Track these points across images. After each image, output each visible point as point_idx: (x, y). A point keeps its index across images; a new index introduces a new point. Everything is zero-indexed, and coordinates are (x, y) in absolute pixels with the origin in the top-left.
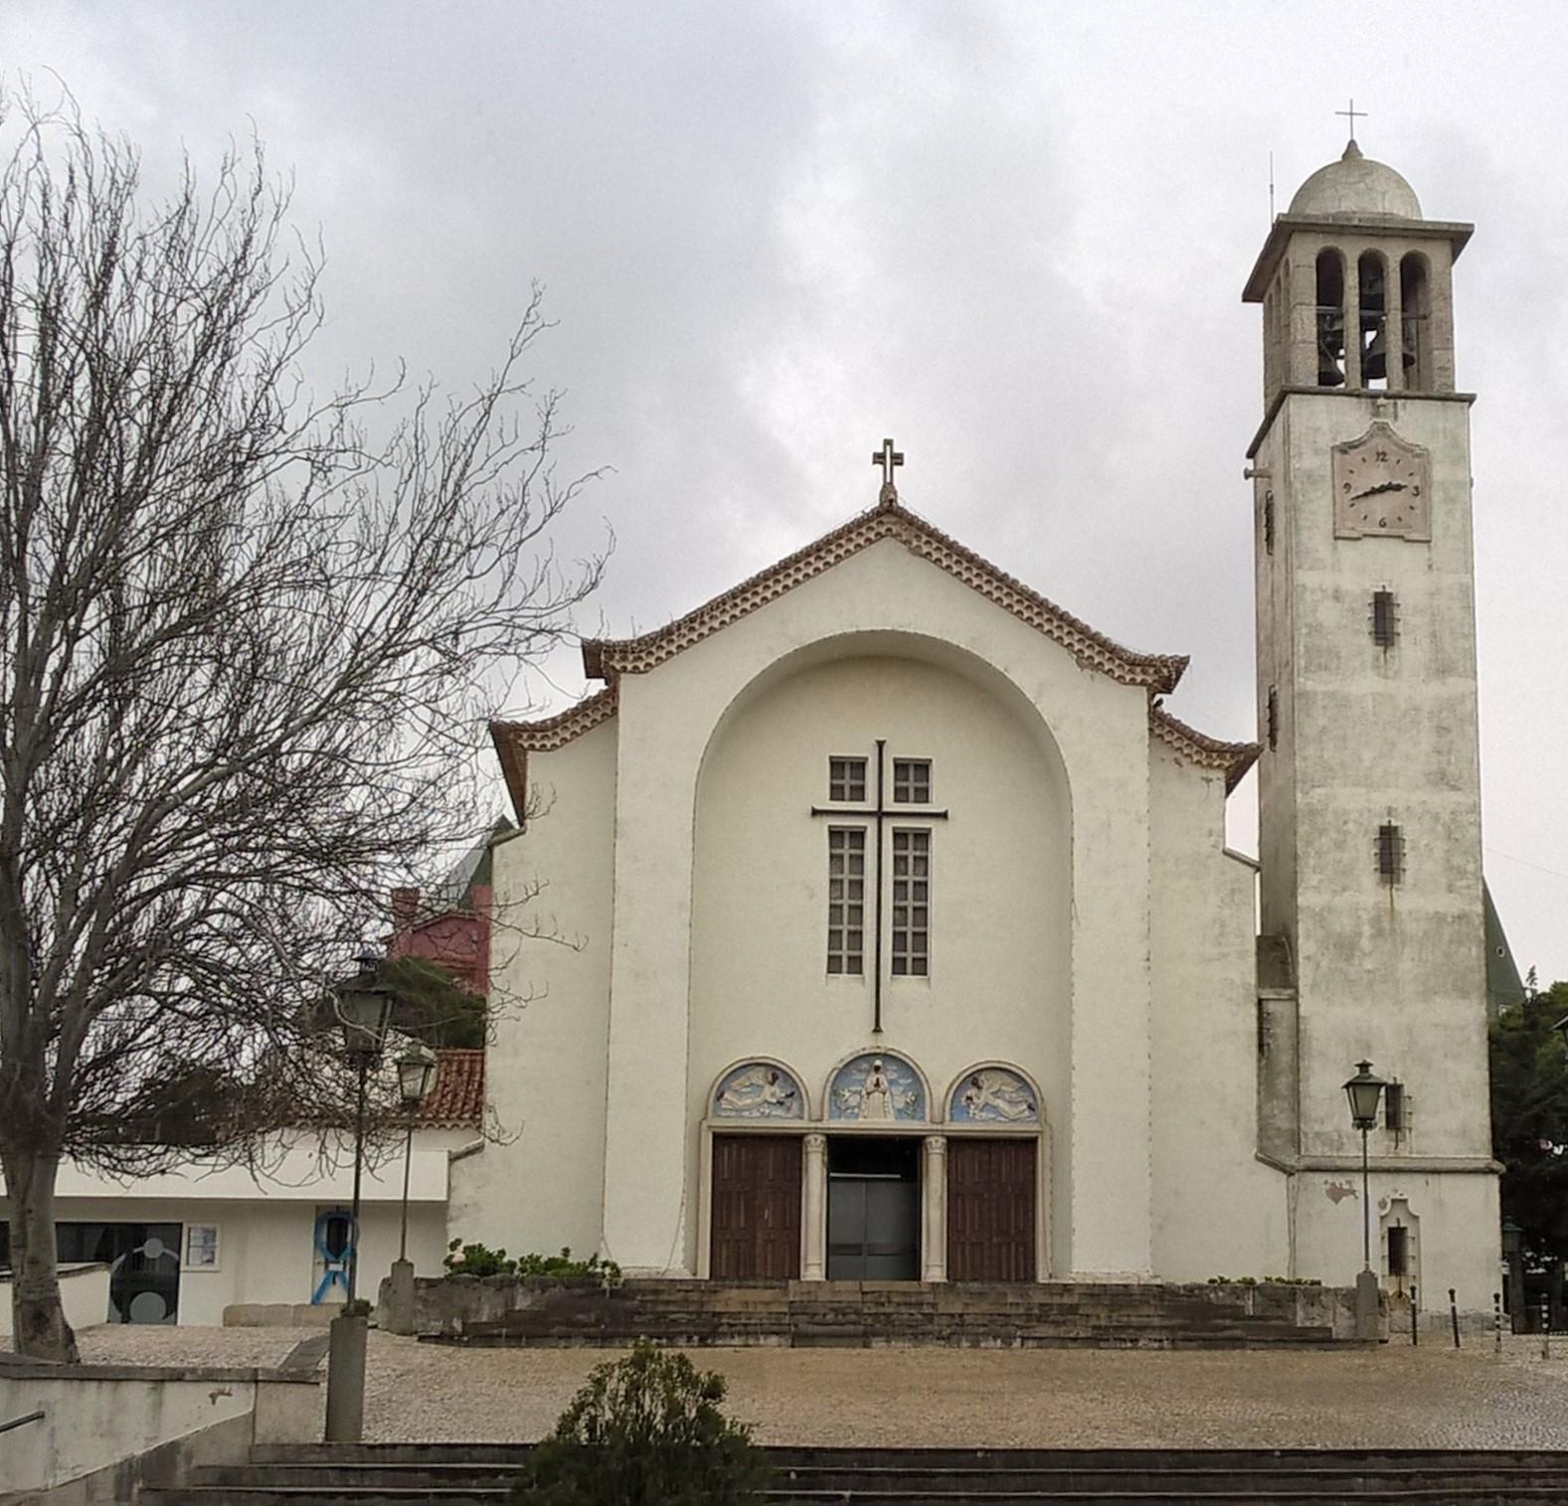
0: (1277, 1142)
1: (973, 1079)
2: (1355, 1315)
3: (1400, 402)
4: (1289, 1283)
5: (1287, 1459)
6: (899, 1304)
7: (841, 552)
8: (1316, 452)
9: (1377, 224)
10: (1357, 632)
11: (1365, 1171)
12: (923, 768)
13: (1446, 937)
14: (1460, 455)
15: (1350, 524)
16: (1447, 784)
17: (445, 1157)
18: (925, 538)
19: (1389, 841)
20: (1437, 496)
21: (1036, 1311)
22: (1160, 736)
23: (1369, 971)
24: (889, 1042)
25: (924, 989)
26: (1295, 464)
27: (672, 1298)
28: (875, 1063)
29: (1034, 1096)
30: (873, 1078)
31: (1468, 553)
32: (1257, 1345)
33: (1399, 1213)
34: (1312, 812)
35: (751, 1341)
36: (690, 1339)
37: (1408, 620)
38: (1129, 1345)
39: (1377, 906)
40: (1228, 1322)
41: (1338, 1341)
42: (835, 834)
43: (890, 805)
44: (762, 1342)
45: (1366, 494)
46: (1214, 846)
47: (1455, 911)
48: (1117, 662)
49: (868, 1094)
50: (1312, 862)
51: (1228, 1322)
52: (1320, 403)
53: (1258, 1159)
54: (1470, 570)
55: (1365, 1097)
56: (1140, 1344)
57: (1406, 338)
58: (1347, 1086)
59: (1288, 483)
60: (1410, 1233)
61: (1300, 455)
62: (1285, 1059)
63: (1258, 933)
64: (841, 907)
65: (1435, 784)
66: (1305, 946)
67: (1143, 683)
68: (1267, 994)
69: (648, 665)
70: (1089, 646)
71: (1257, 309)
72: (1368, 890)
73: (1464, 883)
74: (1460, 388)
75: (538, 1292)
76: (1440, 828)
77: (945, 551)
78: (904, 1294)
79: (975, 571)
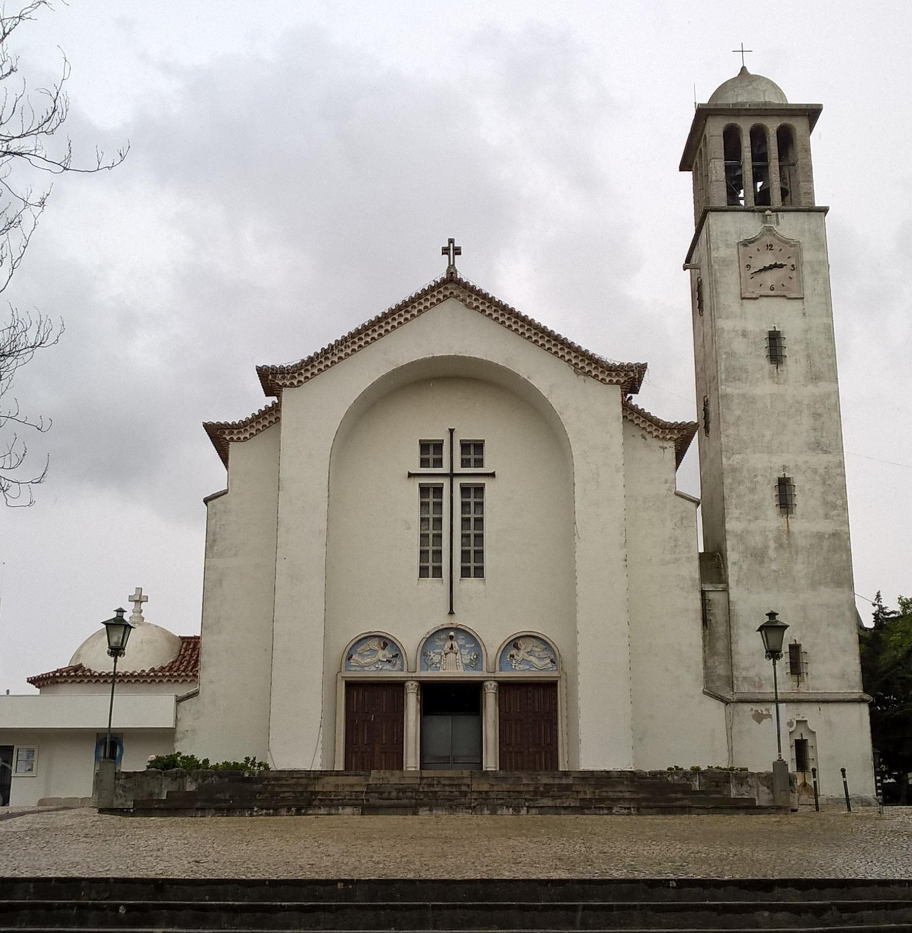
0: (718, 684)
1: (514, 643)
2: (773, 791)
3: (780, 214)
4: (725, 769)
5: (686, 890)
6: (444, 785)
7: (422, 308)
8: (727, 246)
9: (761, 107)
10: (758, 356)
11: (777, 701)
12: (479, 446)
13: (825, 548)
14: (820, 244)
15: (751, 290)
16: (822, 450)
17: (172, 700)
18: (474, 297)
19: (784, 487)
20: (806, 270)
21: (541, 789)
22: (632, 421)
23: (774, 571)
24: (459, 620)
25: (482, 586)
26: (714, 254)
27: (289, 782)
28: (450, 633)
29: (555, 655)
30: (449, 644)
31: (828, 304)
32: (701, 811)
33: (802, 730)
34: (734, 470)
35: (333, 811)
36: (289, 809)
37: (791, 347)
38: (606, 812)
39: (778, 530)
40: (679, 796)
41: (760, 807)
42: (424, 490)
43: (458, 469)
44: (340, 811)
45: (761, 271)
46: (669, 490)
47: (830, 531)
48: (600, 370)
49: (446, 654)
50: (734, 501)
51: (679, 796)
52: (729, 217)
53: (705, 693)
54: (830, 315)
55: (773, 636)
56: (614, 811)
57: (782, 178)
58: (760, 630)
59: (710, 266)
60: (810, 743)
61: (718, 248)
62: (721, 629)
63: (701, 550)
64: (428, 535)
65: (814, 450)
66: (732, 556)
67: (617, 383)
68: (708, 587)
69: (300, 382)
70: (582, 360)
71: (689, 175)
72: (772, 519)
73: (835, 513)
74: (818, 203)
75: (200, 781)
76: (817, 478)
77: (487, 304)
78: (450, 778)
79: (507, 316)
